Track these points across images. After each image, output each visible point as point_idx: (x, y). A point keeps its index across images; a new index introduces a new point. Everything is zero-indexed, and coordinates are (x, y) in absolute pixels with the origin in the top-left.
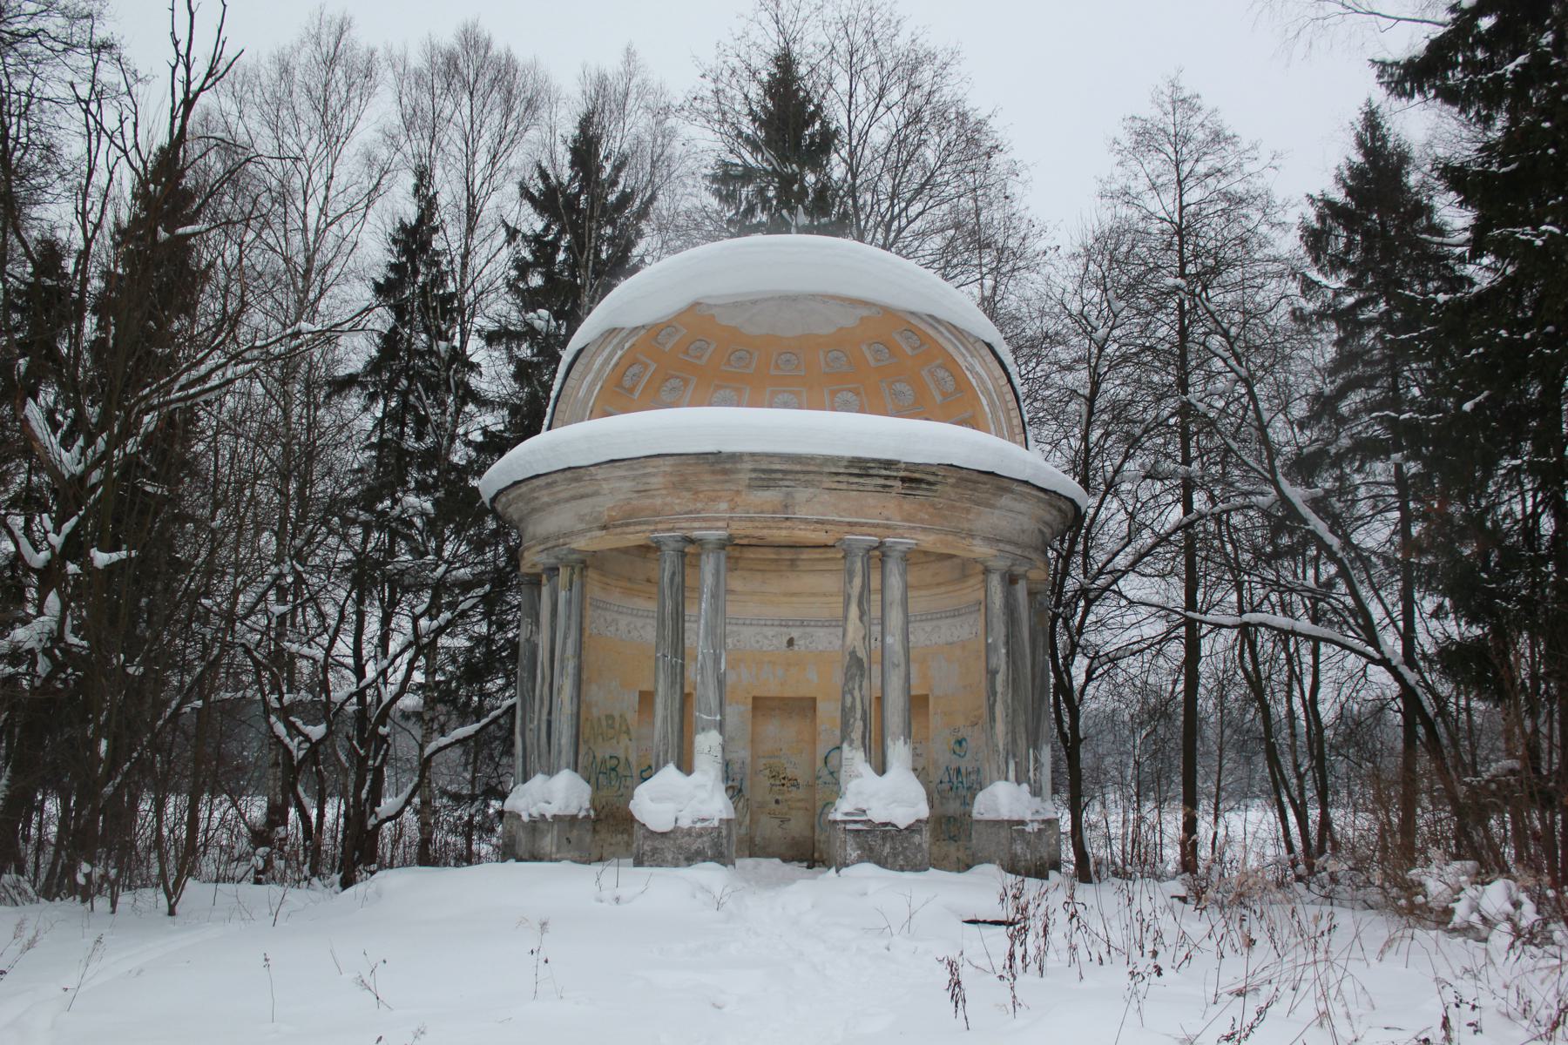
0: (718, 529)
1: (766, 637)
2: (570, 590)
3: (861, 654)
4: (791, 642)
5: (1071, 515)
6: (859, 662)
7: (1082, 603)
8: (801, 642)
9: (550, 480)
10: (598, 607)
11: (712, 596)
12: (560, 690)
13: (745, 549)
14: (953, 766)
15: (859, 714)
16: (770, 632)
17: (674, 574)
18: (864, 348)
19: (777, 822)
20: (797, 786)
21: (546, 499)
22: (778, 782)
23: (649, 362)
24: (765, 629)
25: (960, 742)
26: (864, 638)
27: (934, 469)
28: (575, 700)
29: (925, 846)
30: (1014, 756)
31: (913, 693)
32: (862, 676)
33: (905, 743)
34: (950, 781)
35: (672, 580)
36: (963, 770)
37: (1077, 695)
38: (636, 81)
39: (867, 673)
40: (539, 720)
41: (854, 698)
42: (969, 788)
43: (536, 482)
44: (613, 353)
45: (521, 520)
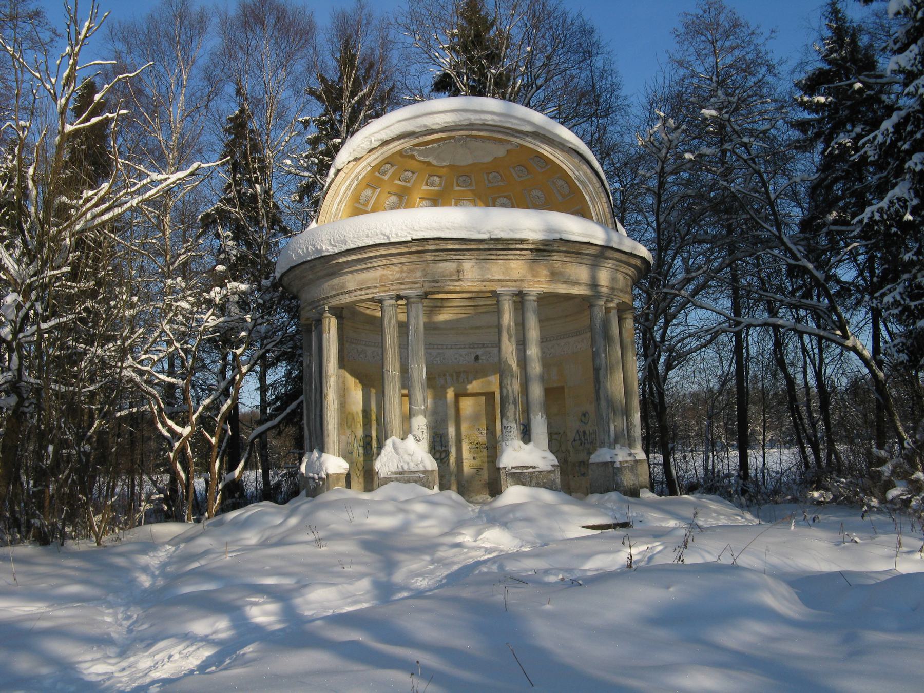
0: (416, 289)
1: (461, 356)
4: (477, 358)
5: (643, 267)
7: (661, 321)
8: (484, 358)
9: (311, 265)
10: (353, 343)
13: (444, 301)
14: (581, 430)
16: (463, 352)
18: (512, 170)
21: (310, 277)
23: (474, 184)
24: (461, 350)
25: (584, 415)
27: (551, 243)
33: (542, 417)
34: (580, 439)
36: (587, 432)
37: (661, 380)
38: (365, 12)
40: (315, 415)
41: (508, 391)
42: (592, 443)
43: (304, 267)
44: (352, 181)
45: (298, 292)
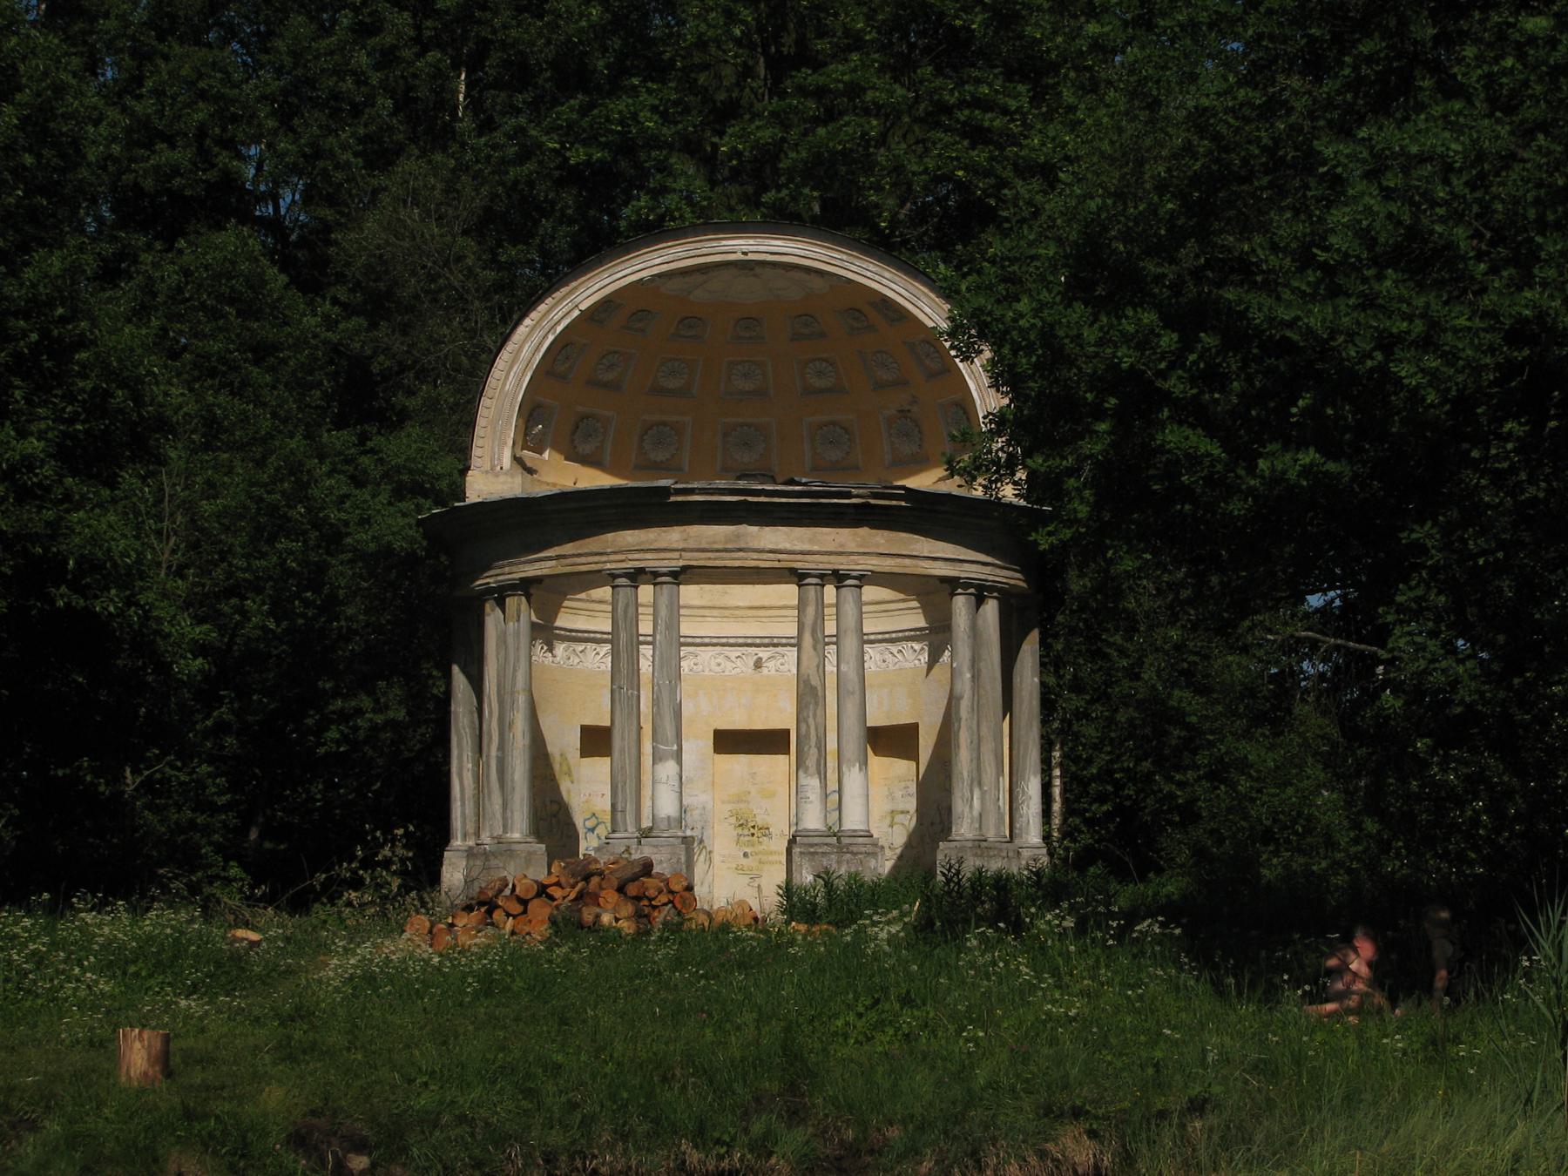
2: (518, 620)
3: (815, 682)
4: (758, 664)
6: (814, 689)
11: (667, 628)
12: (511, 725)
15: (813, 743)
17: (627, 605)
19: (746, 880)
20: (769, 836)
22: (746, 832)
26: (818, 666)
28: (975, 762)
29: (155, 388)
30: (980, 784)
31: (872, 722)
32: (816, 703)
35: (626, 612)
39: (821, 700)
41: (808, 726)
